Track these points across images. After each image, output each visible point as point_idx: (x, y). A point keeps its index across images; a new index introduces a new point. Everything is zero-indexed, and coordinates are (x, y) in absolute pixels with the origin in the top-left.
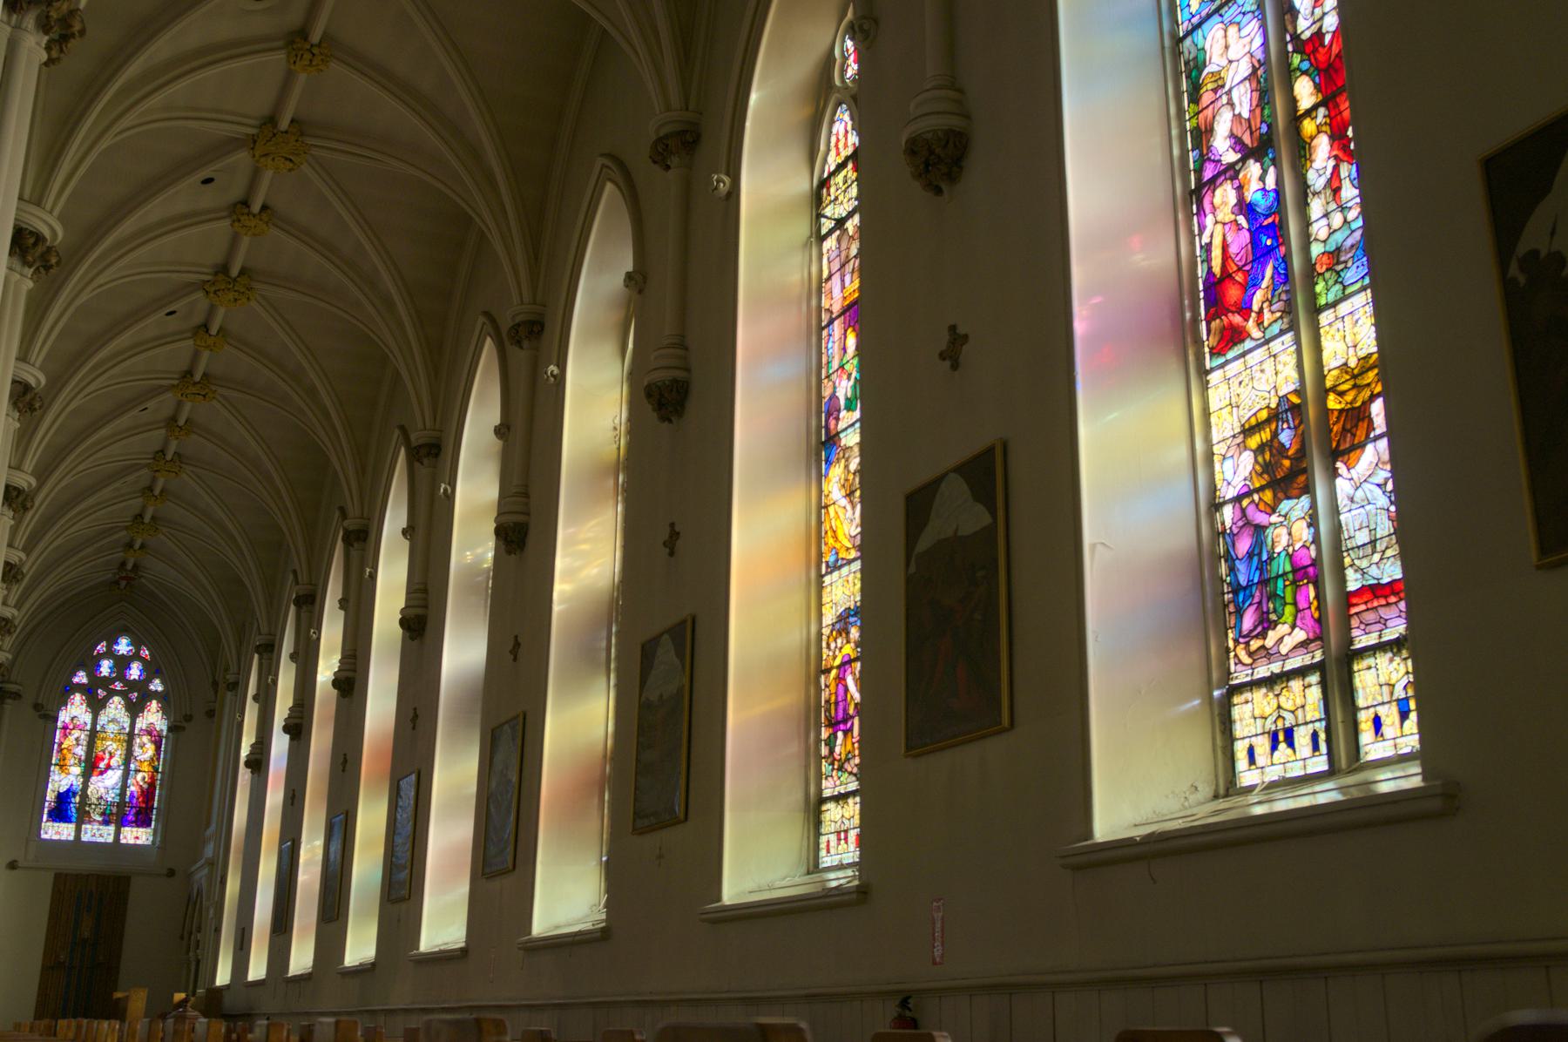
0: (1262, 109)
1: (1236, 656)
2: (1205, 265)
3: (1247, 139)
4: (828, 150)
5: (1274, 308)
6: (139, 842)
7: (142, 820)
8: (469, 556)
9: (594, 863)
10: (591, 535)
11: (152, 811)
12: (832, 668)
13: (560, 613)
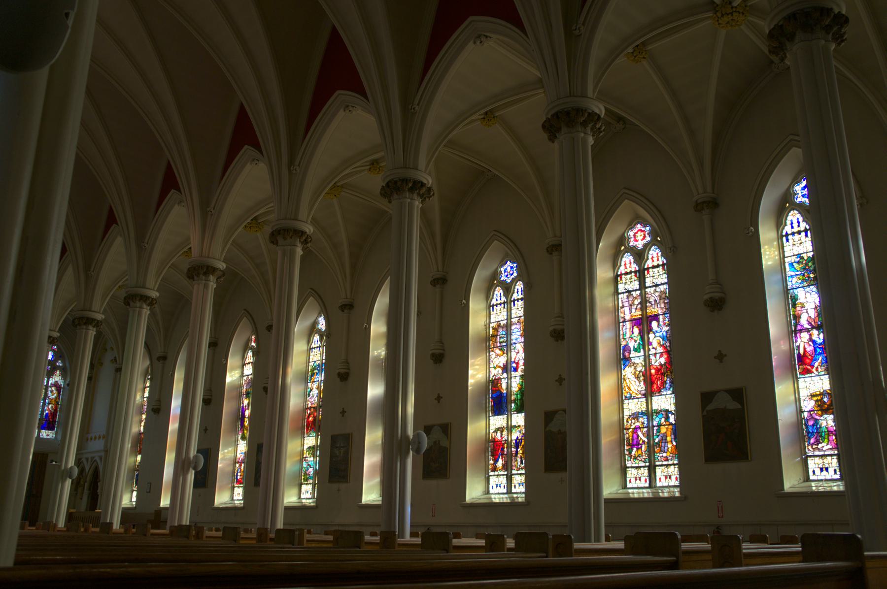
0: (819, 318)
1: (808, 448)
2: (797, 351)
3: (813, 323)
4: (312, 342)
5: (822, 368)
6: (48, 437)
7: (50, 427)
8: (376, 353)
9: (483, 477)
10: (479, 363)
11: (55, 423)
12: (630, 428)
13: (472, 390)
